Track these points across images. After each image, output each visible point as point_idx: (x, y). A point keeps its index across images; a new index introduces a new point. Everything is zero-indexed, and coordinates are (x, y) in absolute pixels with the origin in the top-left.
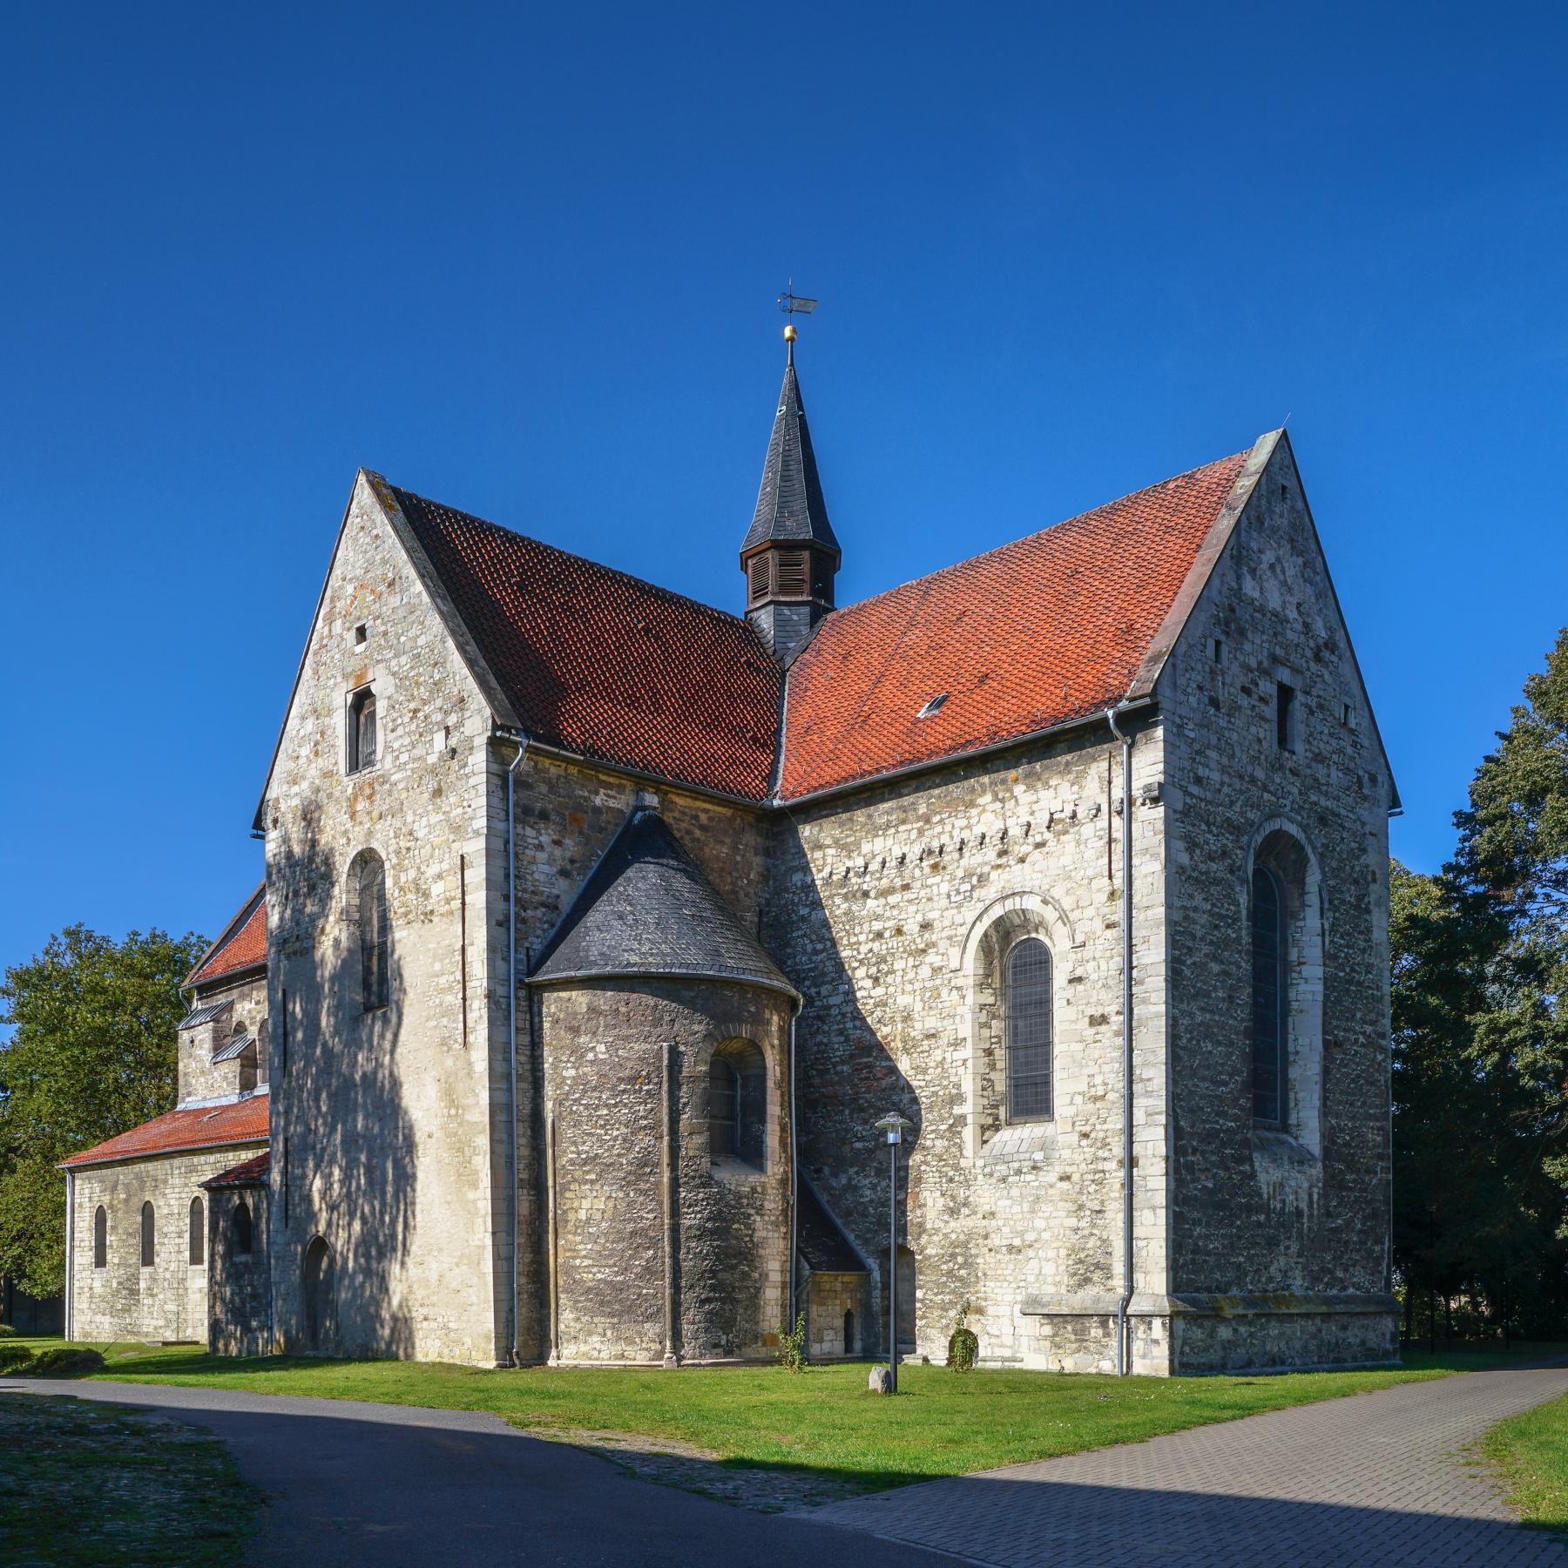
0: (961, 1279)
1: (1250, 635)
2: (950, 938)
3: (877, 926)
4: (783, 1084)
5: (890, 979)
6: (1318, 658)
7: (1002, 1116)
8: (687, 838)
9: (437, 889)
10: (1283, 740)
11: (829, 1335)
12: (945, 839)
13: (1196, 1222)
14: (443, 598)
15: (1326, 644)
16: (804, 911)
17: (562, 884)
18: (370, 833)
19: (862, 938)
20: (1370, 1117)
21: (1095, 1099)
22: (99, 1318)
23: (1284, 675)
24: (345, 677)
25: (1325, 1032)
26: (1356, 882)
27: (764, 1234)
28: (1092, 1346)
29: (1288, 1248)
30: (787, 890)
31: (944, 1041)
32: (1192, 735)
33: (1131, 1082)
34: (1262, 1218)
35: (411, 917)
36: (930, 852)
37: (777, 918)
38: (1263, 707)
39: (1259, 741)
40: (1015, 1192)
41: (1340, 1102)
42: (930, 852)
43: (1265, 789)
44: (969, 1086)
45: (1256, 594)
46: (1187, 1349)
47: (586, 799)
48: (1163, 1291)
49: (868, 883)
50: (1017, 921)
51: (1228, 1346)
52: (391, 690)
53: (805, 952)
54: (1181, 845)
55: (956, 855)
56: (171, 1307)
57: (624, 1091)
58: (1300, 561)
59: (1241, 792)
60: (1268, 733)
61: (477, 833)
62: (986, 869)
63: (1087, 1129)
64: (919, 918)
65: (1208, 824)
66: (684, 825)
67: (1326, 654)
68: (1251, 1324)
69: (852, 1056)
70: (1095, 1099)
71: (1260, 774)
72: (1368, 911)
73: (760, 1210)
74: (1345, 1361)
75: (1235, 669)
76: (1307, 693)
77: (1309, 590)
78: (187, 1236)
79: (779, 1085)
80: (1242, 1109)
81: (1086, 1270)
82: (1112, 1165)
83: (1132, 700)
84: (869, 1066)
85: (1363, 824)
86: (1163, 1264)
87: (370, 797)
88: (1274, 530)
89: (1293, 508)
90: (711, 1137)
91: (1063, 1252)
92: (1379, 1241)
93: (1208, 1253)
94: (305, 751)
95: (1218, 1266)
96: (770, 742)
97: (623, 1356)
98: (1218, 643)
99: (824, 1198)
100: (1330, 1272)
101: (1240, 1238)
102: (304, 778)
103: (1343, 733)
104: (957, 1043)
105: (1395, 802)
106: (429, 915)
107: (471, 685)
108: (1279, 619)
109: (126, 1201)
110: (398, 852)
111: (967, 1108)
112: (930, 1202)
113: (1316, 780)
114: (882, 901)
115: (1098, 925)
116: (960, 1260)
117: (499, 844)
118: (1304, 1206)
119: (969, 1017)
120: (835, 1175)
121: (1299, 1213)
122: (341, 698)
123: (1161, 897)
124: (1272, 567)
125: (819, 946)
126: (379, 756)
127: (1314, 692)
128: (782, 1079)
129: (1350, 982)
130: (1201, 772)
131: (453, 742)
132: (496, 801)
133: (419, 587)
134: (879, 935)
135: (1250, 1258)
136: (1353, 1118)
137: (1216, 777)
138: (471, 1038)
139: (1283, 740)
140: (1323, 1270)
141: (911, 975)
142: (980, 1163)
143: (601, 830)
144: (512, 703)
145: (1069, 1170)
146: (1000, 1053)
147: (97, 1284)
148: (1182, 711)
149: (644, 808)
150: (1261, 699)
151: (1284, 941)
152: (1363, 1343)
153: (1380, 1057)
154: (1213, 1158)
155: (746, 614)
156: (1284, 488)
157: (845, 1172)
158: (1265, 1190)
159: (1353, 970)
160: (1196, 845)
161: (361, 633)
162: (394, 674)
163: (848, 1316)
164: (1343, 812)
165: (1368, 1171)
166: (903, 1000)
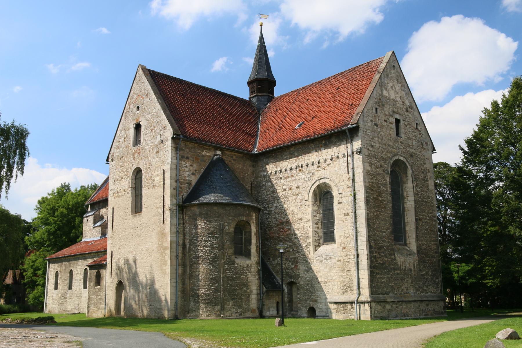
0: (310, 291)
1: (386, 106)
2: (305, 191)
3: (284, 187)
4: (257, 234)
5: (288, 202)
6: (407, 111)
7: (321, 243)
8: (229, 163)
9: (157, 179)
10: (398, 134)
11: (272, 309)
12: (303, 163)
13: (377, 274)
14: (161, 99)
15: (409, 107)
16: (264, 183)
17: (193, 177)
18: (138, 163)
19: (280, 191)
20: (432, 241)
21: (347, 237)
22: (54, 306)
23: (397, 116)
24: (133, 120)
25: (416, 216)
26: (423, 173)
27: (251, 278)
28: (349, 312)
29: (407, 281)
30: (259, 177)
31: (303, 221)
32: (370, 134)
33: (356, 232)
34: (399, 272)
35: (149, 187)
36: (299, 166)
37: (256, 185)
38: (391, 125)
39: (390, 134)
40: (325, 265)
41: (422, 237)
42: (299, 166)
43: (393, 148)
44: (311, 234)
45: (387, 95)
46: (376, 312)
47: (200, 153)
48: (368, 295)
49: (281, 175)
50: (323, 186)
51: (390, 311)
52: (146, 124)
53: (264, 195)
54: (368, 164)
55: (306, 167)
56: (77, 302)
57: (209, 237)
58: (400, 85)
59: (386, 149)
60: (394, 132)
61: (168, 163)
62: (314, 171)
63: (344, 246)
64: (296, 185)
65: (376, 158)
66: (228, 159)
67: (409, 110)
68: (396, 304)
69: (278, 225)
70: (347, 237)
71: (391, 144)
72: (427, 181)
73: (250, 271)
74: (428, 315)
75: (382, 115)
76: (404, 121)
77: (403, 93)
78: (82, 280)
79: (255, 234)
80: (391, 240)
81: (346, 289)
82: (352, 257)
83: (351, 125)
84: (283, 228)
85: (424, 156)
86: (367, 286)
87: (139, 153)
88: (392, 77)
89: (397, 71)
90: (235, 250)
91: (339, 283)
92: (438, 278)
93: (382, 283)
94: (122, 140)
95: (385, 287)
96: (254, 135)
97: (208, 316)
98: (376, 109)
99: (271, 267)
100: (422, 288)
101: (392, 278)
102: (121, 147)
103: (416, 131)
104: (308, 221)
105: (434, 149)
106: (154, 186)
107: (167, 123)
108: (395, 101)
109: (65, 269)
110: (146, 169)
111: (311, 240)
112: (301, 268)
113: (409, 144)
114: (286, 180)
115: (345, 187)
116: (310, 285)
117: (174, 166)
118: (412, 268)
119: (310, 213)
120: (274, 260)
121: (411, 270)
122: (132, 126)
123: (362, 179)
124: (392, 87)
125: (268, 193)
126: (142, 142)
127: (407, 120)
128: (257, 232)
129: (423, 201)
130: (373, 144)
131: (162, 138)
132: (173, 155)
133: (154, 96)
134: (285, 190)
135: (395, 284)
136: (426, 241)
137: (377, 145)
138: (165, 221)
139: (398, 134)
140: (419, 287)
141: (294, 201)
142: (315, 256)
143: (204, 161)
144: (179, 127)
145: (340, 258)
146: (320, 224)
147: (54, 296)
148: (366, 127)
149: (217, 155)
150: (390, 123)
151: (402, 190)
152: (434, 310)
153: (434, 223)
154: (382, 254)
155: (249, 98)
156: (394, 66)
157: (276, 259)
158: (399, 263)
159: (424, 198)
160: (372, 164)
161: (138, 108)
162: (146, 119)
163: (278, 303)
164: (417, 153)
165: (432, 257)
166: (292, 209)
